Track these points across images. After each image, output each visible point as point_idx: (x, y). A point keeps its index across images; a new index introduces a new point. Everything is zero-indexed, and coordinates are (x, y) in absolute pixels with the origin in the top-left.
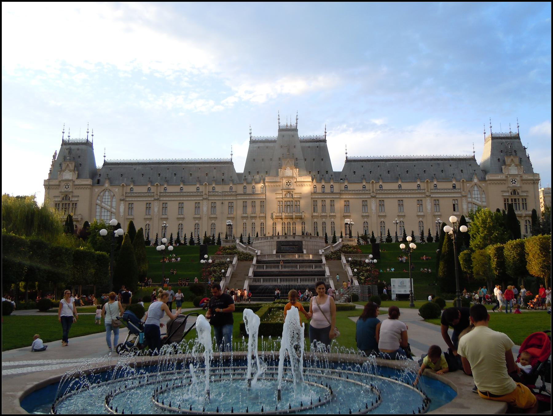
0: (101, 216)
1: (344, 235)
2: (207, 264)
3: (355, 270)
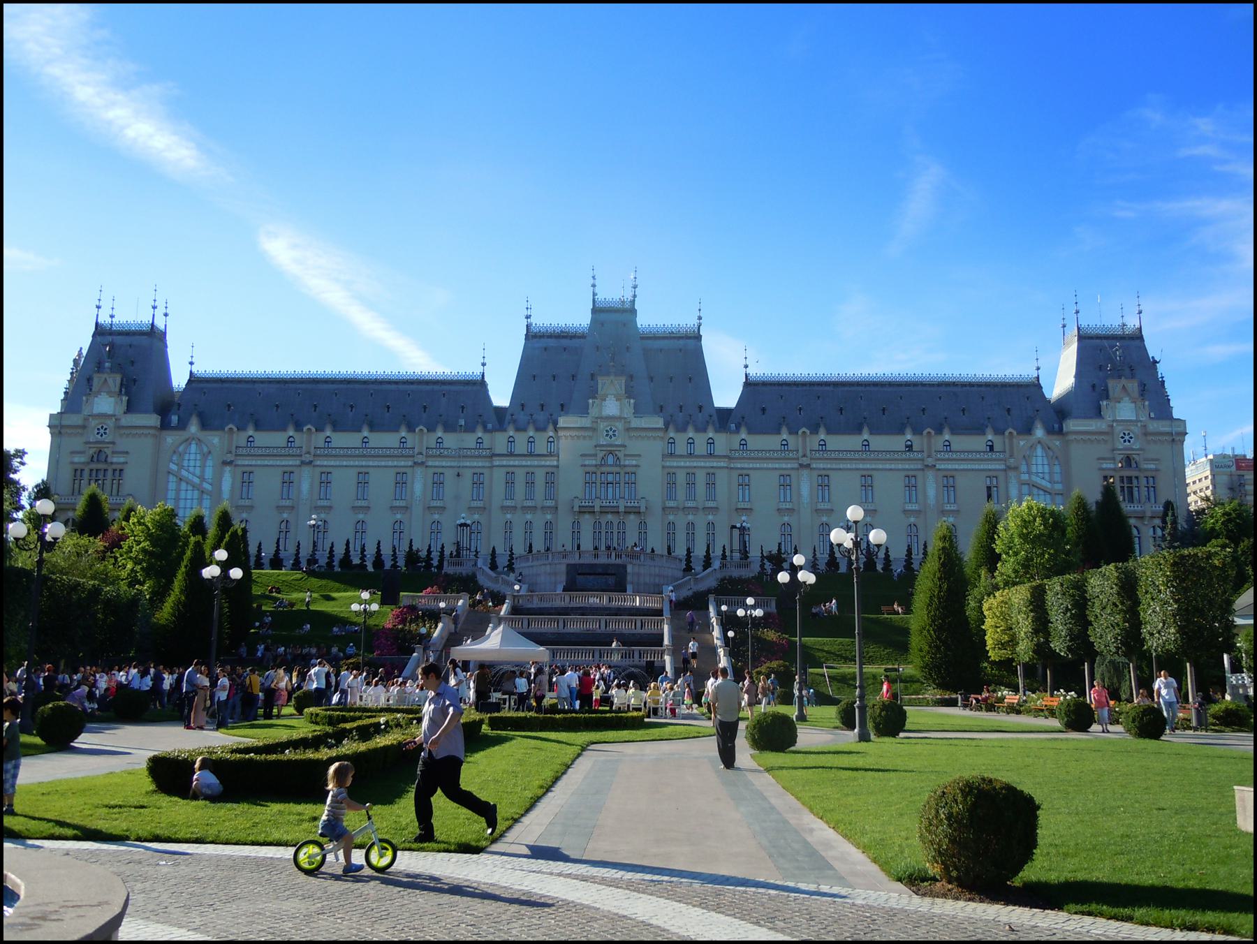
0: (177, 499)
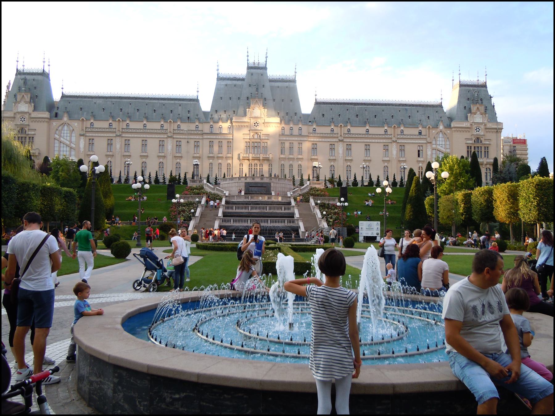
0: (59, 151)
1: (311, 178)
2: (178, 203)
3: (324, 213)
